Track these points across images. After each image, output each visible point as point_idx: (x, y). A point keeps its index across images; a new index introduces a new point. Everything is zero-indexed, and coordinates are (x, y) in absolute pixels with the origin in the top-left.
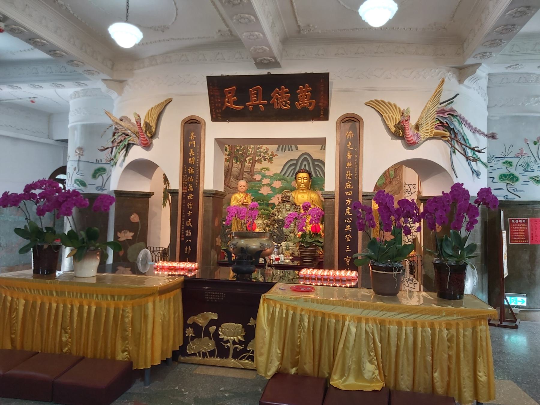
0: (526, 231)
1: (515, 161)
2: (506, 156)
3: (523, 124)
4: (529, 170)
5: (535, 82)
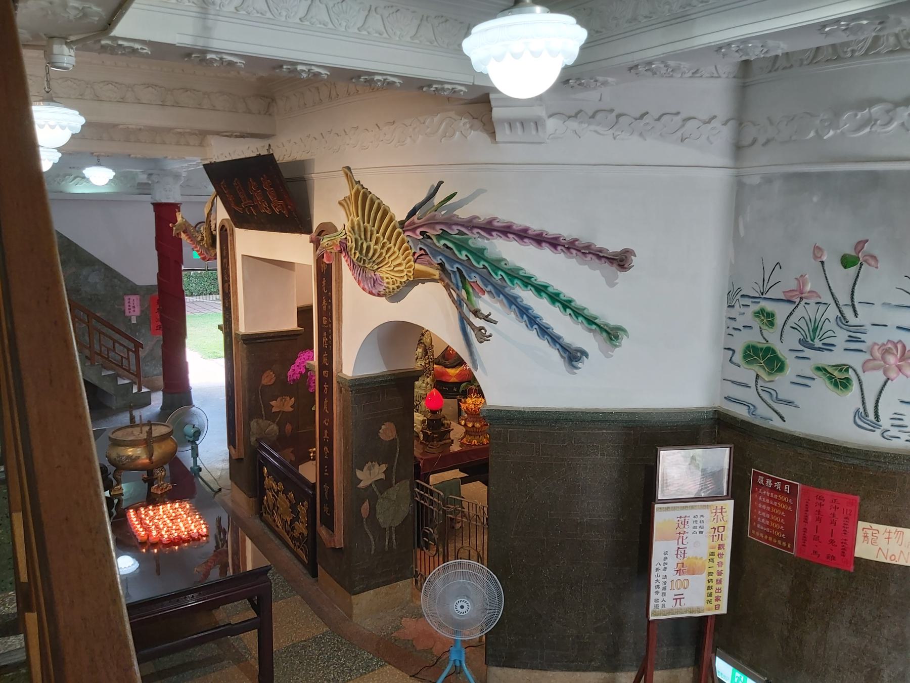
0: (790, 516)
1: (781, 311)
2: (762, 295)
3: (815, 199)
4: (818, 344)
5: (866, 54)
